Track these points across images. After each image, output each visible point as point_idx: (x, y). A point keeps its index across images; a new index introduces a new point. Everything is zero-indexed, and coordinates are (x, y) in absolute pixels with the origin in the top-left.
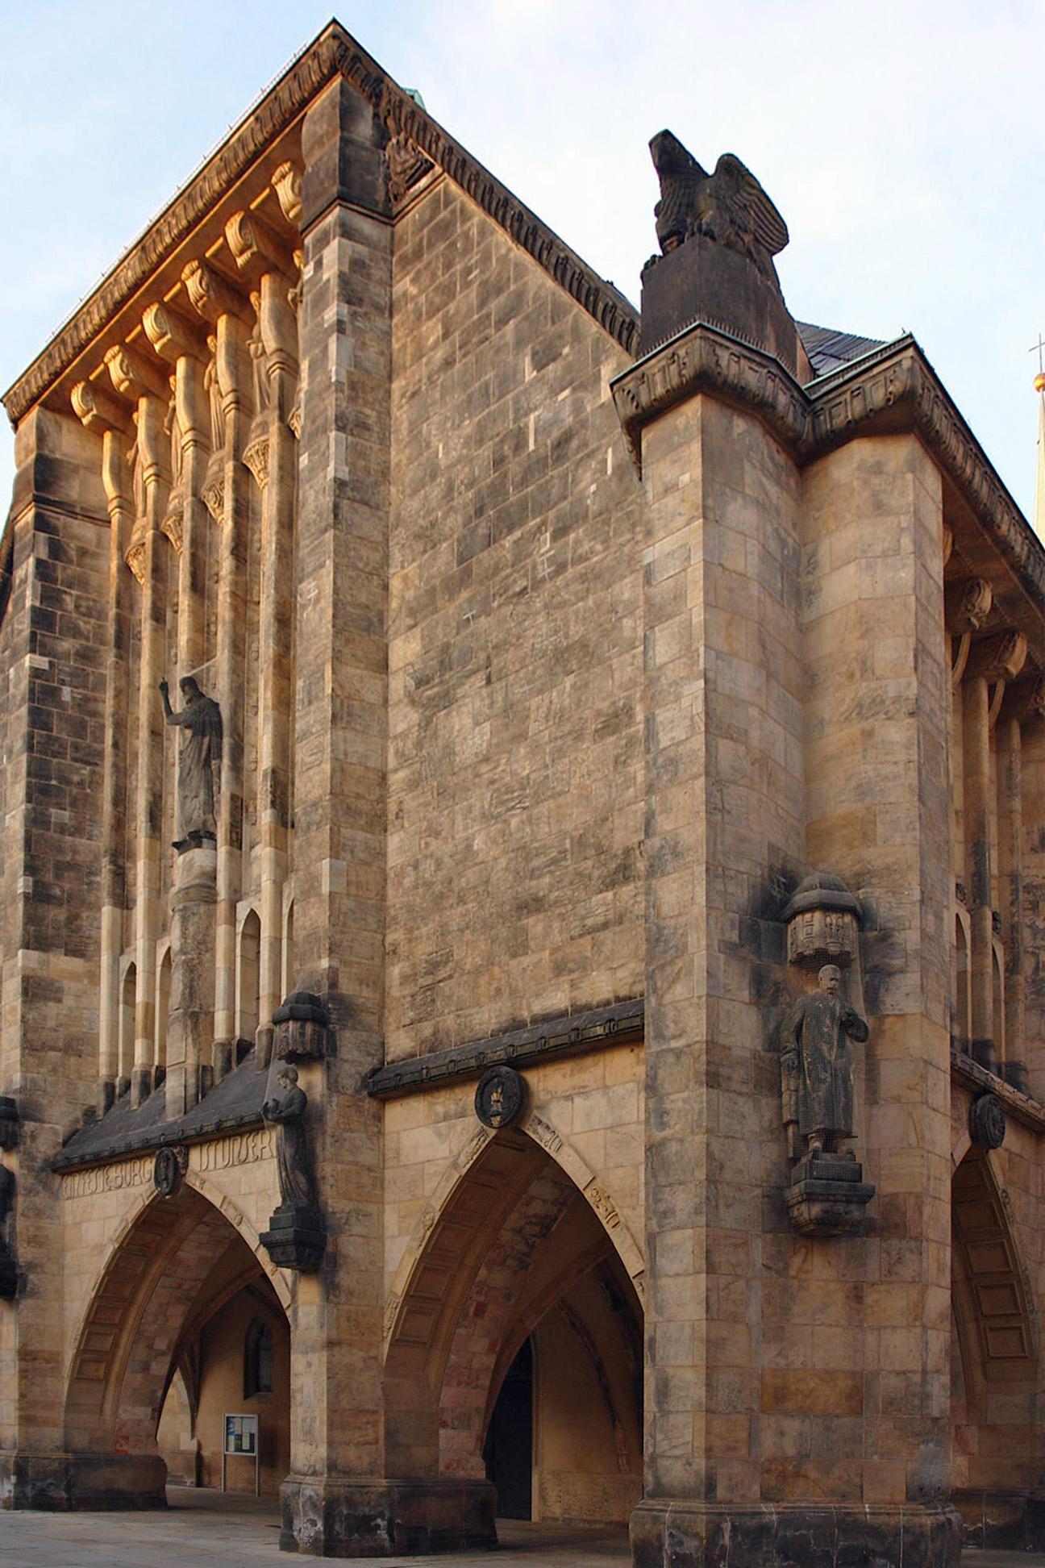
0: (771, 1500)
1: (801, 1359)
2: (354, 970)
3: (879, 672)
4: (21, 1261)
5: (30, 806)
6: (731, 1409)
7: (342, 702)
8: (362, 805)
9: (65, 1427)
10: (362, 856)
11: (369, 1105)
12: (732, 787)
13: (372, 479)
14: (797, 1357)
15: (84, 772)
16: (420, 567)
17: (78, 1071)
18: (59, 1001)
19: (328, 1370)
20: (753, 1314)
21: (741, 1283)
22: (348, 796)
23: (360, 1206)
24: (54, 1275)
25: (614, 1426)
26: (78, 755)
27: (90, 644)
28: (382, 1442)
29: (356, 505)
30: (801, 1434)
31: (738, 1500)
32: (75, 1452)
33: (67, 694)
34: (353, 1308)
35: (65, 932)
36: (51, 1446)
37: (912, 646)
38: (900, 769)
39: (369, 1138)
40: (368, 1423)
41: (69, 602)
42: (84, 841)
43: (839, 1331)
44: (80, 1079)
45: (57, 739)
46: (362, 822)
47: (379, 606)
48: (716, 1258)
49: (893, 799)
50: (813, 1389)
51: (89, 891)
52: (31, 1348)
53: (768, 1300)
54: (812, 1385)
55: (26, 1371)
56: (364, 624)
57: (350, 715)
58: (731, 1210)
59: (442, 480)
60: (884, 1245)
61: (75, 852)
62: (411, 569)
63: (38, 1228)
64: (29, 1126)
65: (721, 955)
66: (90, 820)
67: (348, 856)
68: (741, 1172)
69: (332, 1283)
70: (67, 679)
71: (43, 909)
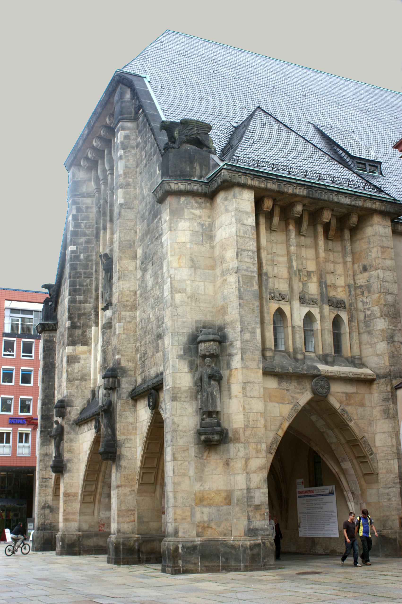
0: (200, 536)
1: (208, 487)
2: (126, 358)
3: (227, 261)
4: (65, 459)
5: (70, 297)
6: (183, 505)
7: (122, 273)
8: (129, 303)
9: (79, 522)
10: (128, 320)
11: (131, 402)
12: (180, 307)
13: (131, 200)
14: (207, 486)
15: (88, 281)
16: (142, 227)
17: (85, 386)
18: (79, 362)
19: (117, 496)
20: (192, 472)
21: (186, 463)
22: (124, 302)
23: (128, 437)
24: (76, 463)
25: (273, 508)
26: (86, 276)
27: (90, 237)
28: (136, 521)
29: (126, 210)
30: (209, 513)
31: (187, 537)
32: (83, 531)
33: (82, 256)
34: (126, 473)
35: (81, 338)
36: (74, 530)
37: (236, 252)
38: (234, 290)
39: (131, 413)
40: (131, 514)
41: (83, 225)
42: (88, 305)
43: (221, 476)
44: (86, 389)
45: (79, 272)
46: (128, 309)
47: (134, 239)
48: (177, 456)
49: (232, 300)
50: (213, 497)
51: (89, 322)
52: (67, 492)
53: (196, 468)
54: (213, 495)
55: (66, 501)
56: (129, 246)
57: (124, 276)
58: (182, 439)
59: (145, 200)
60: (234, 446)
61: (85, 309)
62: (140, 227)
63: (71, 446)
64: (69, 409)
65: (177, 360)
66: (90, 297)
67: (124, 321)
68: (185, 426)
69: (119, 465)
70: (82, 251)
71: (73, 331)
